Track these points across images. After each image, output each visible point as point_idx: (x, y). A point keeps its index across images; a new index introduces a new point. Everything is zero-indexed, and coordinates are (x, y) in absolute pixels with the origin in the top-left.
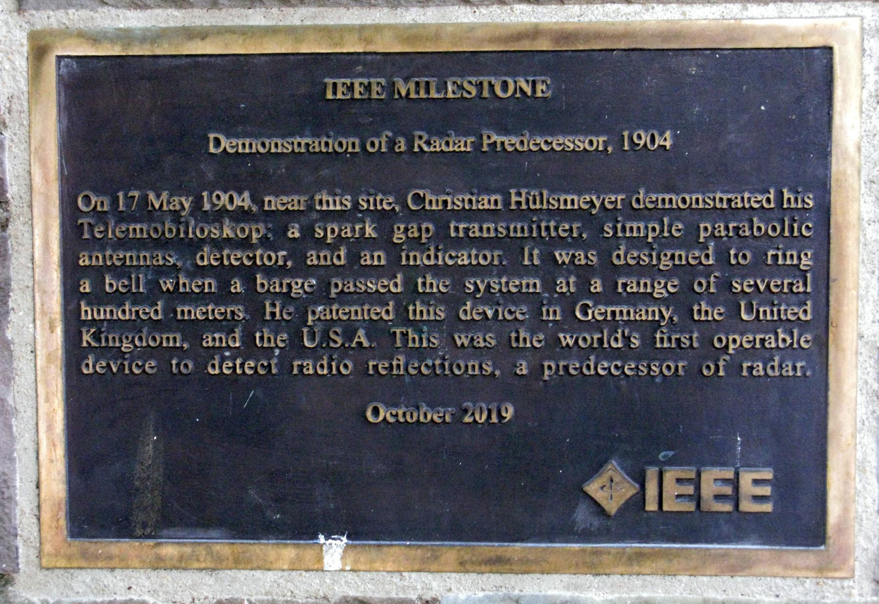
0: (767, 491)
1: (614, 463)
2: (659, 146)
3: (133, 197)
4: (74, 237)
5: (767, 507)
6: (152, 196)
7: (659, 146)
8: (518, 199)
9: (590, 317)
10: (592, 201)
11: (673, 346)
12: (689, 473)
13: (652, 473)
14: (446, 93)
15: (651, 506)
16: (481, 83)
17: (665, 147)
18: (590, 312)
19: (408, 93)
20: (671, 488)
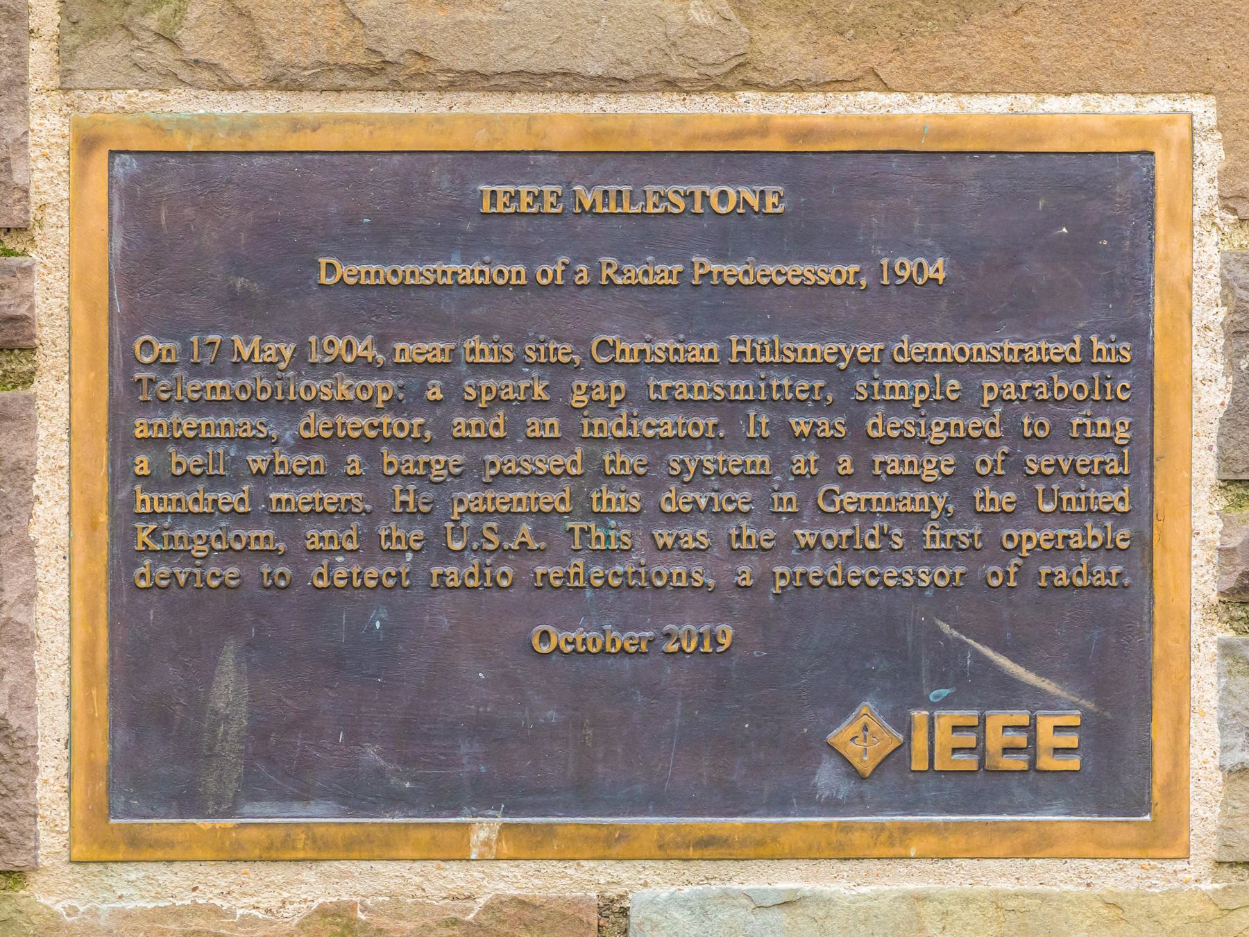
5: (1073, 763)
10: (839, 352)
14: (645, 206)
15: (920, 763)
16: (692, 193)
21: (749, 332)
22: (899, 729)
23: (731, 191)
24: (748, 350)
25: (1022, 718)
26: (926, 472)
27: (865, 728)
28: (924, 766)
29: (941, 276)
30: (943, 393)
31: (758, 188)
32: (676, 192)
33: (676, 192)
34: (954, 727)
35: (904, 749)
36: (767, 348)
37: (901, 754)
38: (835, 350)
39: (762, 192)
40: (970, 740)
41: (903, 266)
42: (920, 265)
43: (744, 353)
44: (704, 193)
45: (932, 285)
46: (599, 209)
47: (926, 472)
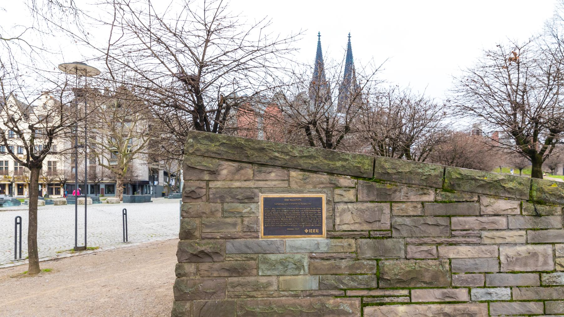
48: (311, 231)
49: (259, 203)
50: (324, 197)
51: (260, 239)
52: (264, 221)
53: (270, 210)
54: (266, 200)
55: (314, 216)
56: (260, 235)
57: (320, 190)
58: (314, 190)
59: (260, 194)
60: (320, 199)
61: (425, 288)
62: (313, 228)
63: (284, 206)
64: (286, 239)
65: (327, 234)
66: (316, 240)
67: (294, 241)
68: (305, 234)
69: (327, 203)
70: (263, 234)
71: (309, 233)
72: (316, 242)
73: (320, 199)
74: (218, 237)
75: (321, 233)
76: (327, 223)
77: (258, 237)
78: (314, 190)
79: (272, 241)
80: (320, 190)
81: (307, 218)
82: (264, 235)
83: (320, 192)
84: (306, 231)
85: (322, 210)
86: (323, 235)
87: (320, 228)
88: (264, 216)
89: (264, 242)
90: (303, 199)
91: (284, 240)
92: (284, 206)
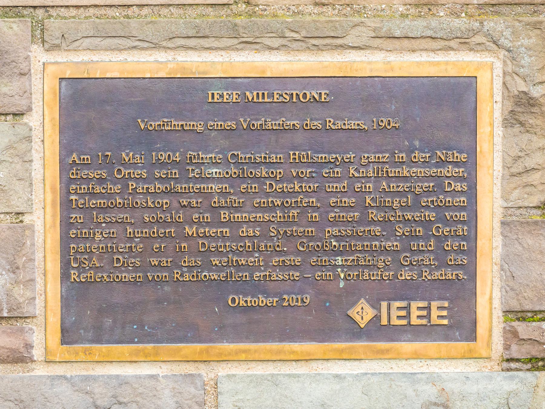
0: (445, 313)
1: (362, 300)
2: (393, 127)
3: (108, 155)
4: (472, 220)
5: (445, 322)
6: (248, 93)
7: (173, 160)
8: (294, 157)
9: (440, 234)
10: (337, 158)
11: (145, 191)
12: (403, 304)
13: (384, 304)
14: (273, 99)
15: (384, 322)
16: (292, 94)
17: (176, 161)
18: (440, 231)
19: (253, 99)
20: (395, 313)
21: (297, 150)
22: (373, 307)
23: (308, 93)
24: (297, 157)
25: (403, 304)
26: (395, 205)
27: (362, 308)
28: (386, 323)
29: (178, 160)
30: (89, 204)
31: (319, 92)
32: (286, 93)
33: (286, 93)
34: (438, 307)
35: (377, 317)
36: (305, 156)
37: (377, 317)
38: (334, 157)
39: (320, 93)
40: (424, 313)
41: (382, 121)
42: (169, 155)
43: (295, 158)
44: (297, 94)
45: (394, 128)
46: (255, 100)
47: (395, 205)
48: (393, 312)
49: (33, 120)
50: (489, 74)
51: (41, 371)
52: (65, 241)
53: (108, 163)
54: (82, 100)
55: (417, 206)
56: (37, 338)
57: (460, 23)
58: (418, 26)
59: (38, 55)
60: (458, 94)
61: (143, 49)
62: (406, 292)
63: (201, 139)
64: (222, 370)
65: (511, 335)
66: (432, 379)
67: (274, 380)
68: (356, 332)
69: (512, 120)
70: (55, 336)
71: (377, 331)
72: (430, 392)
73: (458, 94)
74: (489, 129)
75: (462, 327)
76: (506, 258)
77: (19, 358)
78: (418, 26)
79: (122, 381)
80: (460, 23)
81: (364, 221)
82: (68, 336)
83: (464, 41)
84: (363, 313)
85: (471, 165)
86: (480, 345)
87: (460, 291)
88: (66, 205)
89: (64, 389)
90: (346, 91)
91: (203, 370)
92: (201, 139)
